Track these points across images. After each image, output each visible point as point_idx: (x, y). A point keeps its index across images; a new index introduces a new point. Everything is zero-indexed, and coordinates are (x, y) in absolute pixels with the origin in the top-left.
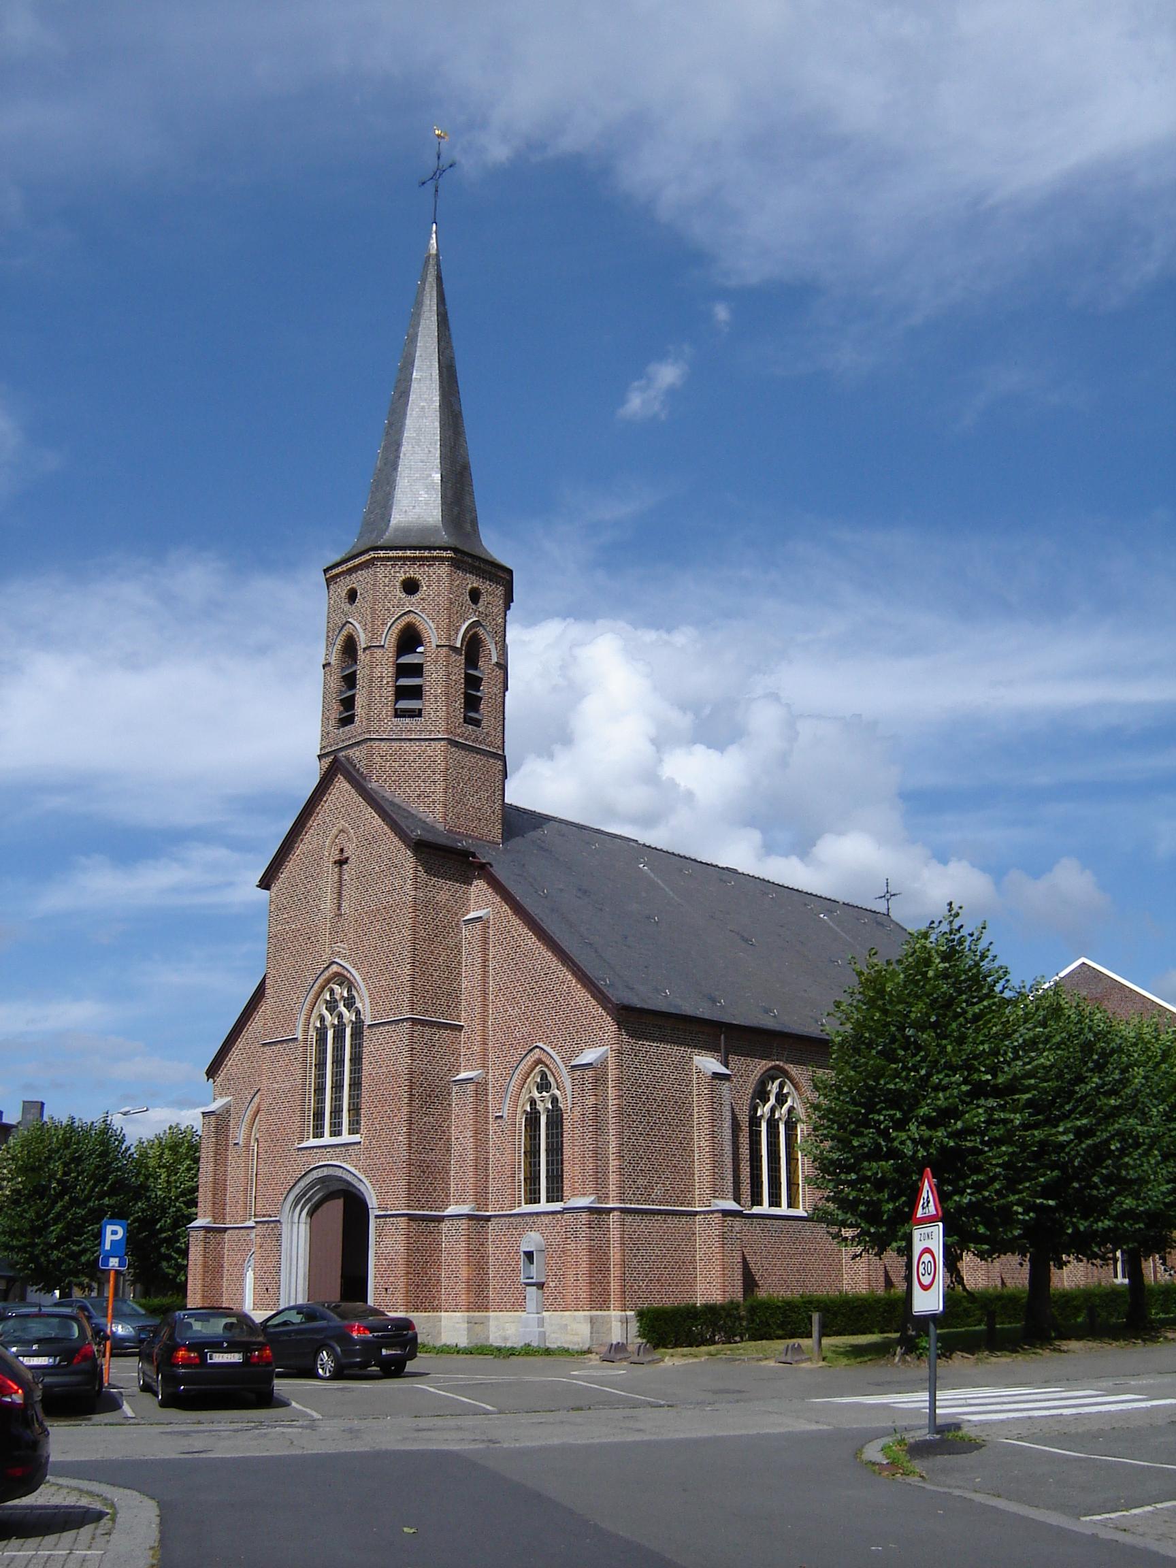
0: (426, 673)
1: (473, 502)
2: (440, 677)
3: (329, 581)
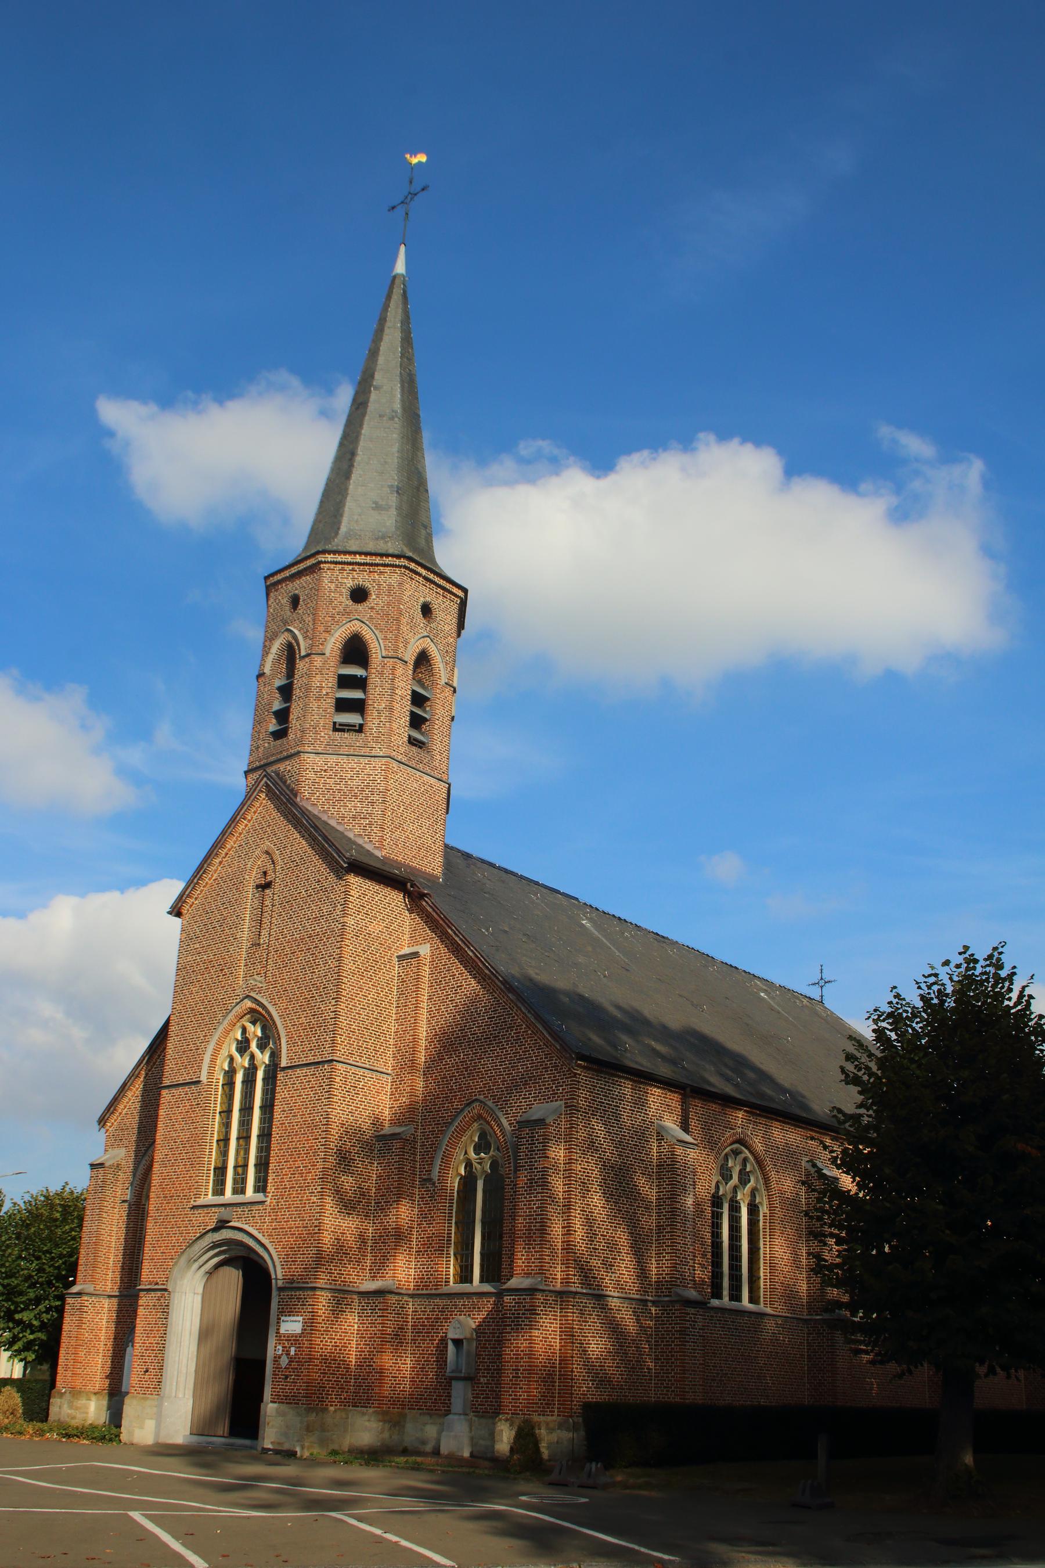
0: (370, 687)
1: (428, 517)
3: (268, 589)
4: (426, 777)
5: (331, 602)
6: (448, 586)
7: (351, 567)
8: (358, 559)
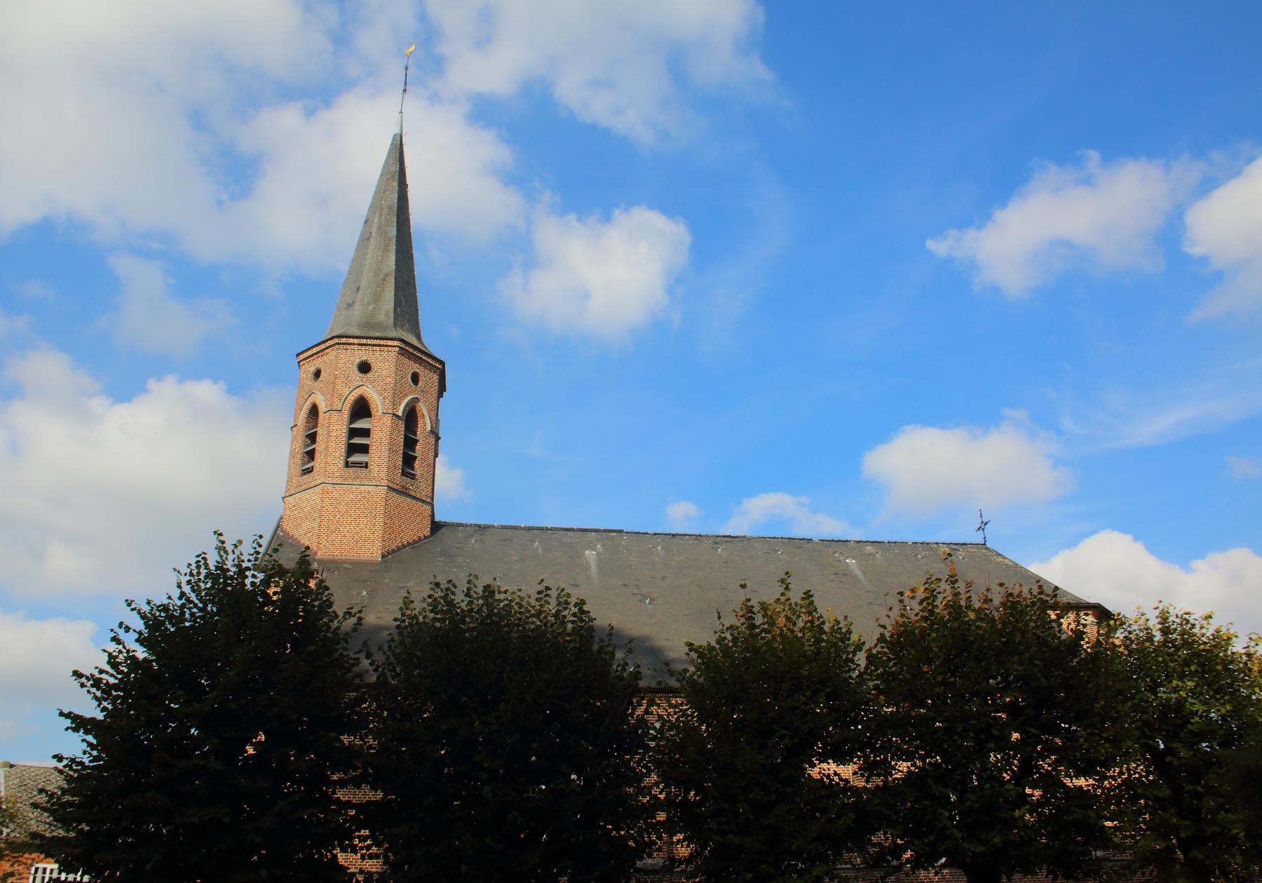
2: (383, 432)
4: (362, 488)
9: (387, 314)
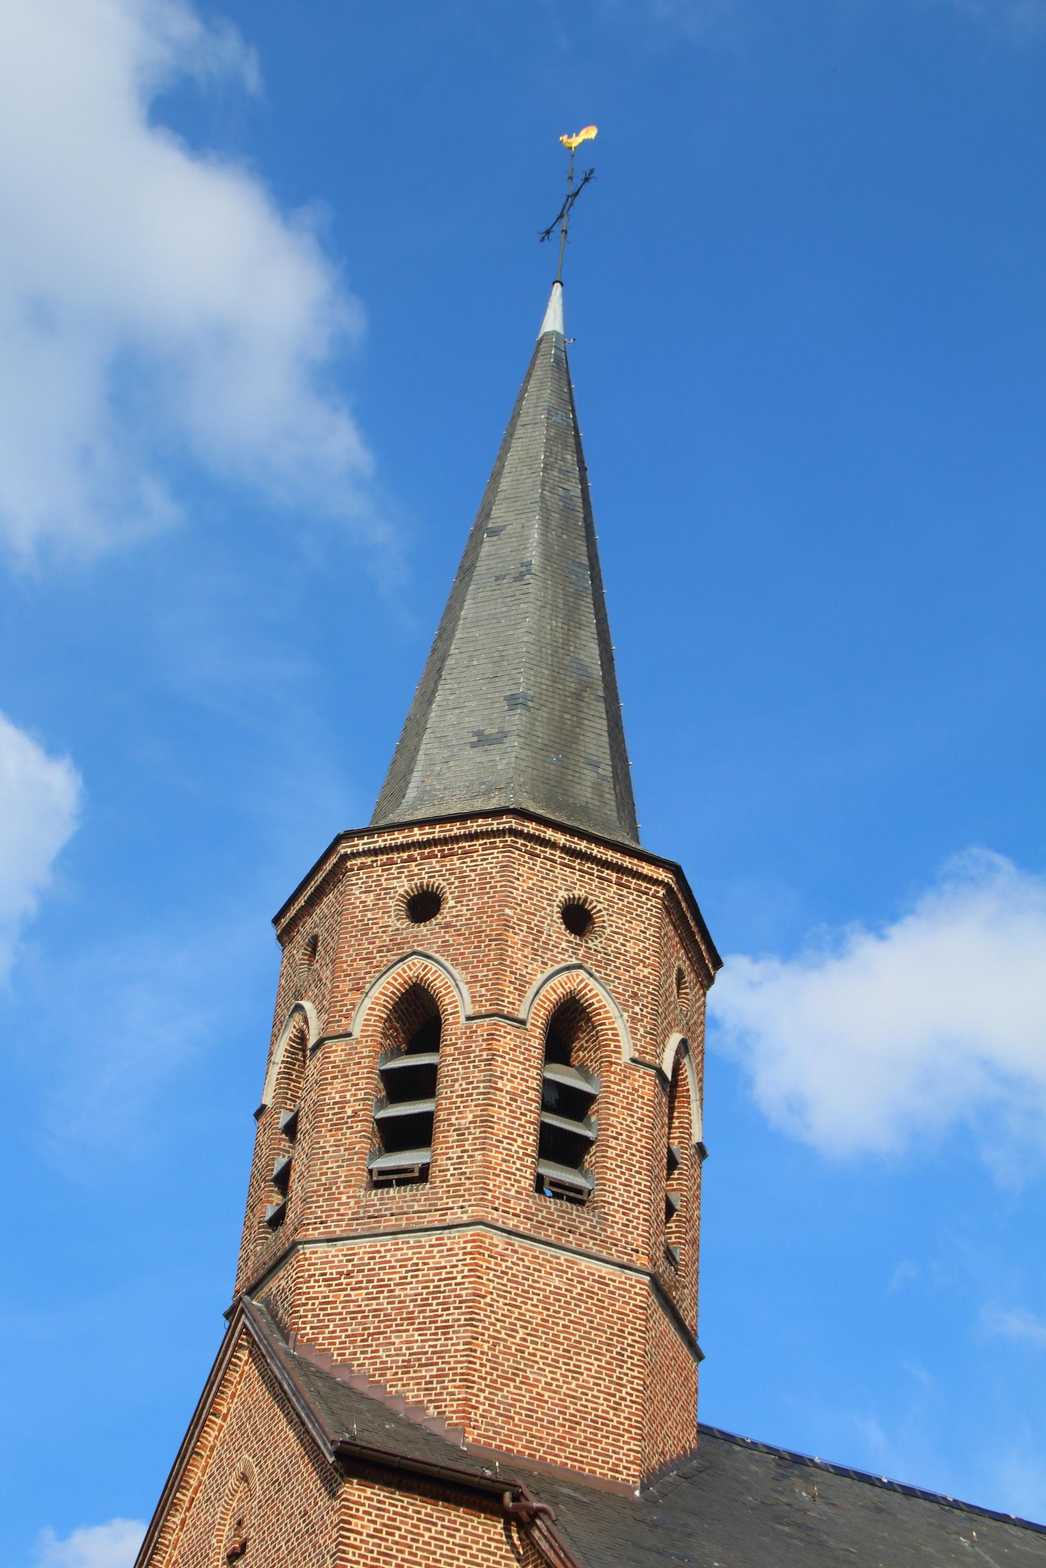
4: (585, 1263)
5: (367, 928)
6: (627, 862)
7: (405, 855)
8: (417, 834)
9: (597, 788)
